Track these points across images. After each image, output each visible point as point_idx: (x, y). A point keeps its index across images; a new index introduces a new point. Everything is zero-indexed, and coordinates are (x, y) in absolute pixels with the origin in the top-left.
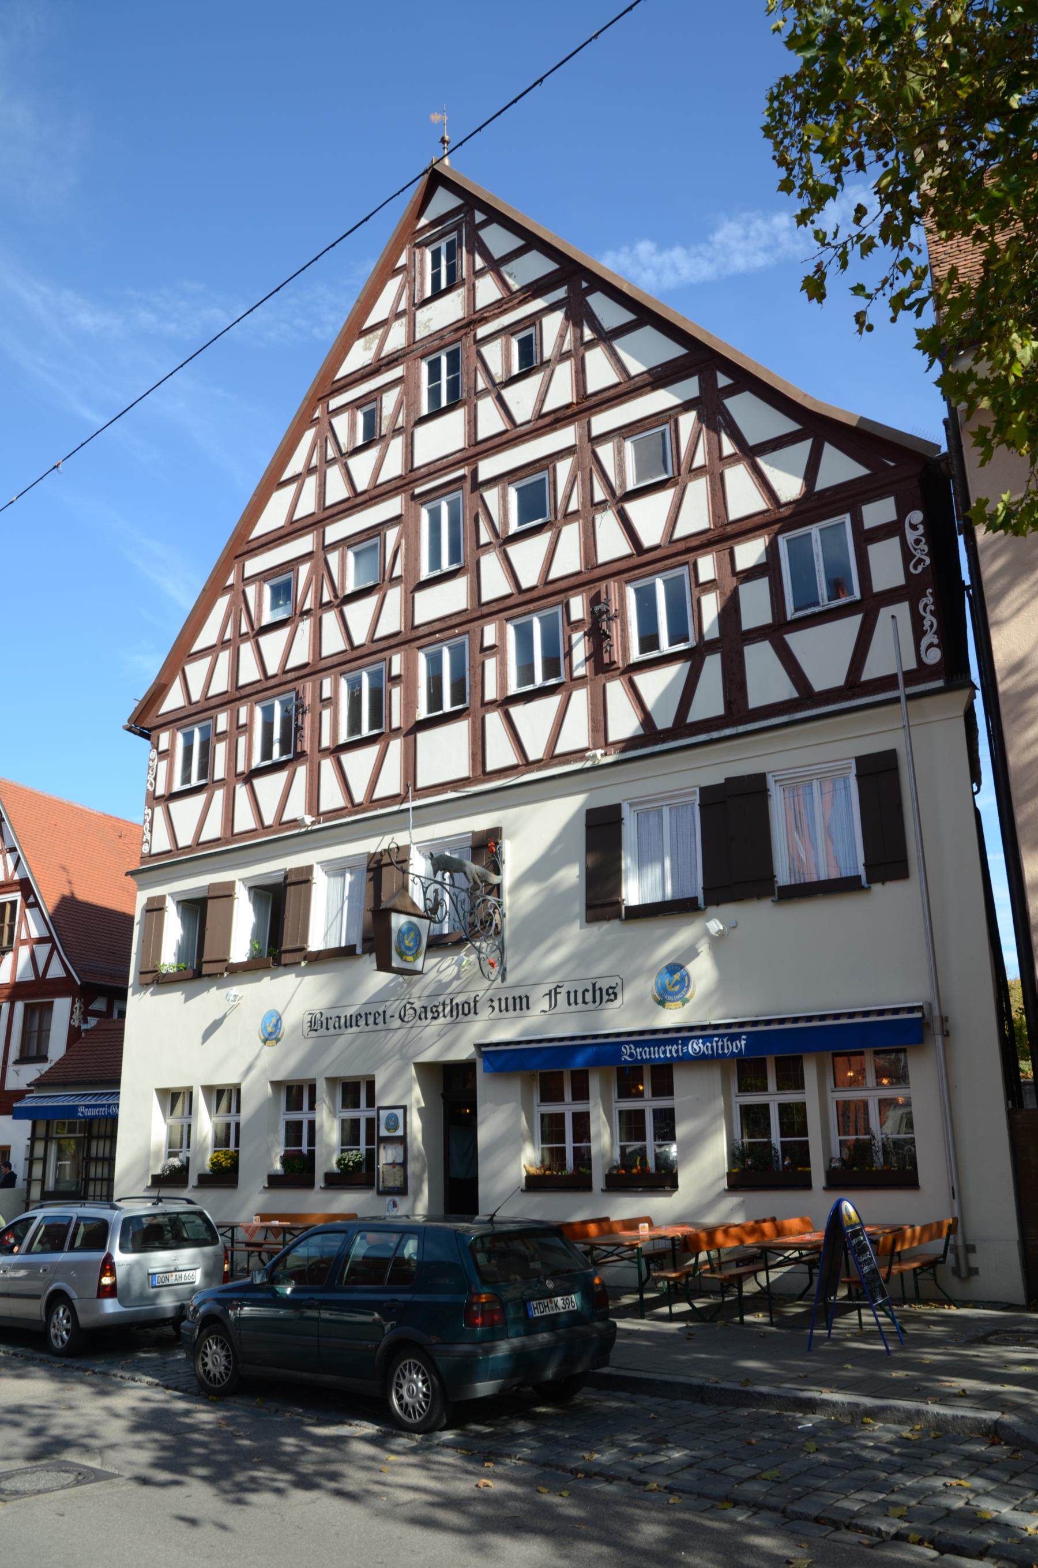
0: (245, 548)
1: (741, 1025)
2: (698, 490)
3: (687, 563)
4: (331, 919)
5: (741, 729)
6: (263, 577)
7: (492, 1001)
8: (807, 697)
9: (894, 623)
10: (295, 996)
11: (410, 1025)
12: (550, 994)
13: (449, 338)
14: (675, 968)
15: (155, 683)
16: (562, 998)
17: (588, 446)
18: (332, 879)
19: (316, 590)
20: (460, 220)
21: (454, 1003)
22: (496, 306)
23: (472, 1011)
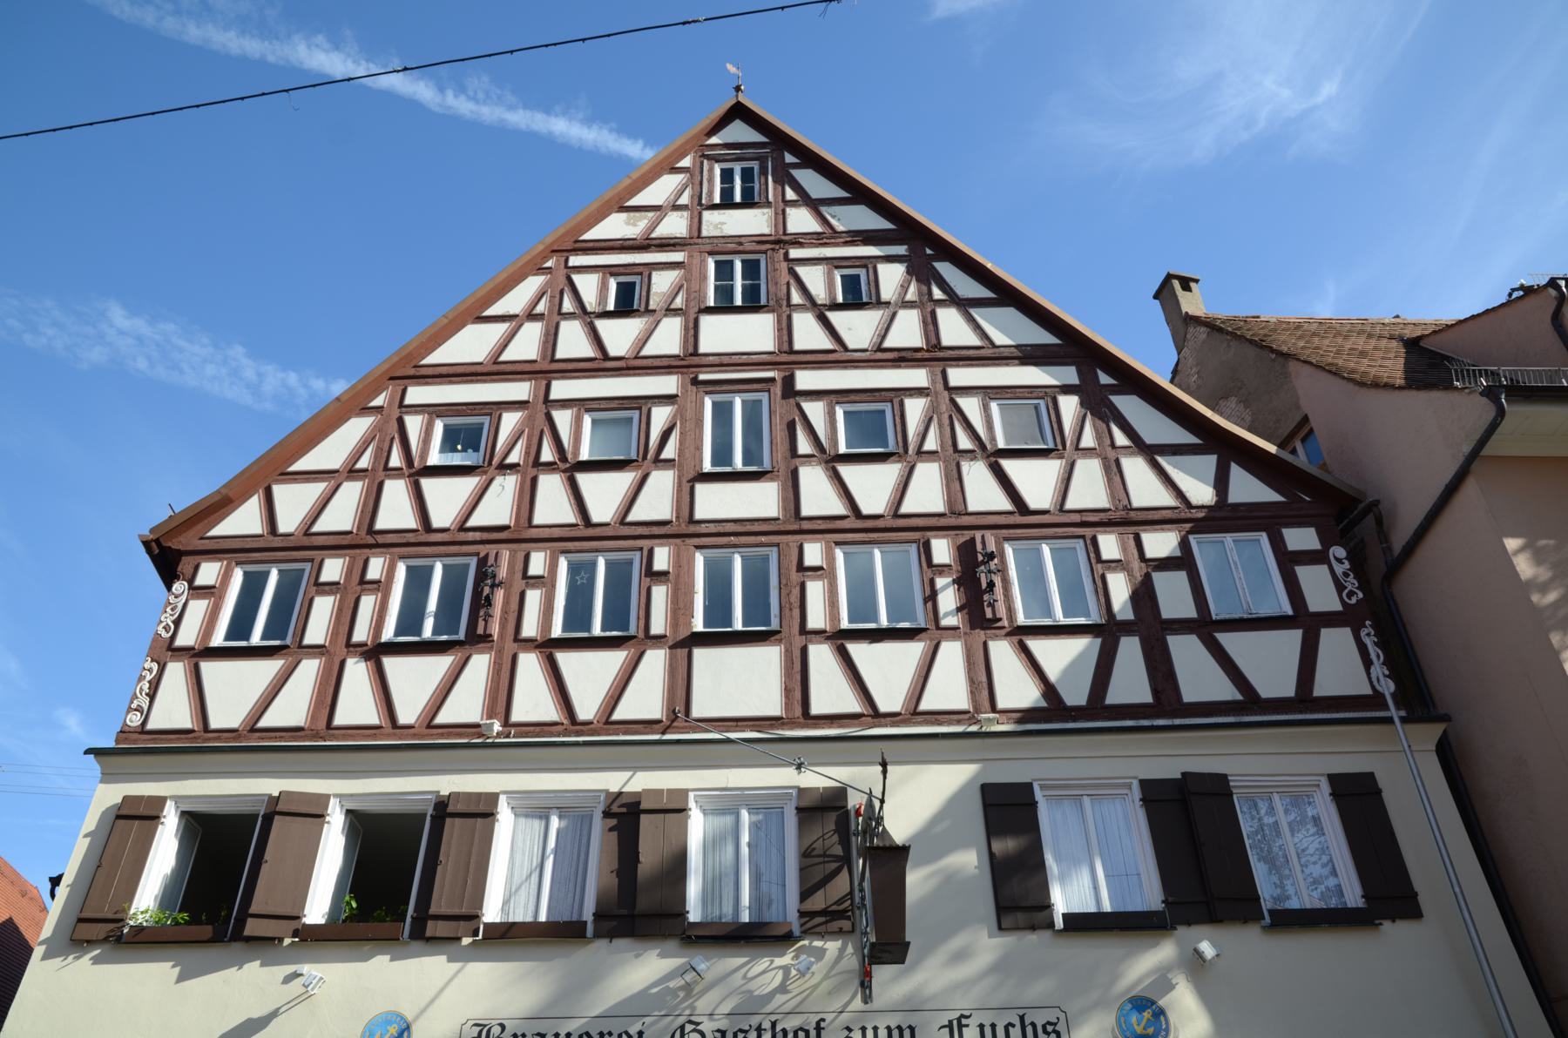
0: (412, 372)
2: (504, 490)
3: (312, 560)
4: (517, 881)
5: (1178, 722)
6: (433, 411)
7: (849, 1029)
9: (1337, 645)
12: (950, 1026)
13: (748, 246)
15: (218, 491)
17: (541, 408)
18: (522, 820)
19: (528, 447)
20: (772, 155)
21: (778, 1028)
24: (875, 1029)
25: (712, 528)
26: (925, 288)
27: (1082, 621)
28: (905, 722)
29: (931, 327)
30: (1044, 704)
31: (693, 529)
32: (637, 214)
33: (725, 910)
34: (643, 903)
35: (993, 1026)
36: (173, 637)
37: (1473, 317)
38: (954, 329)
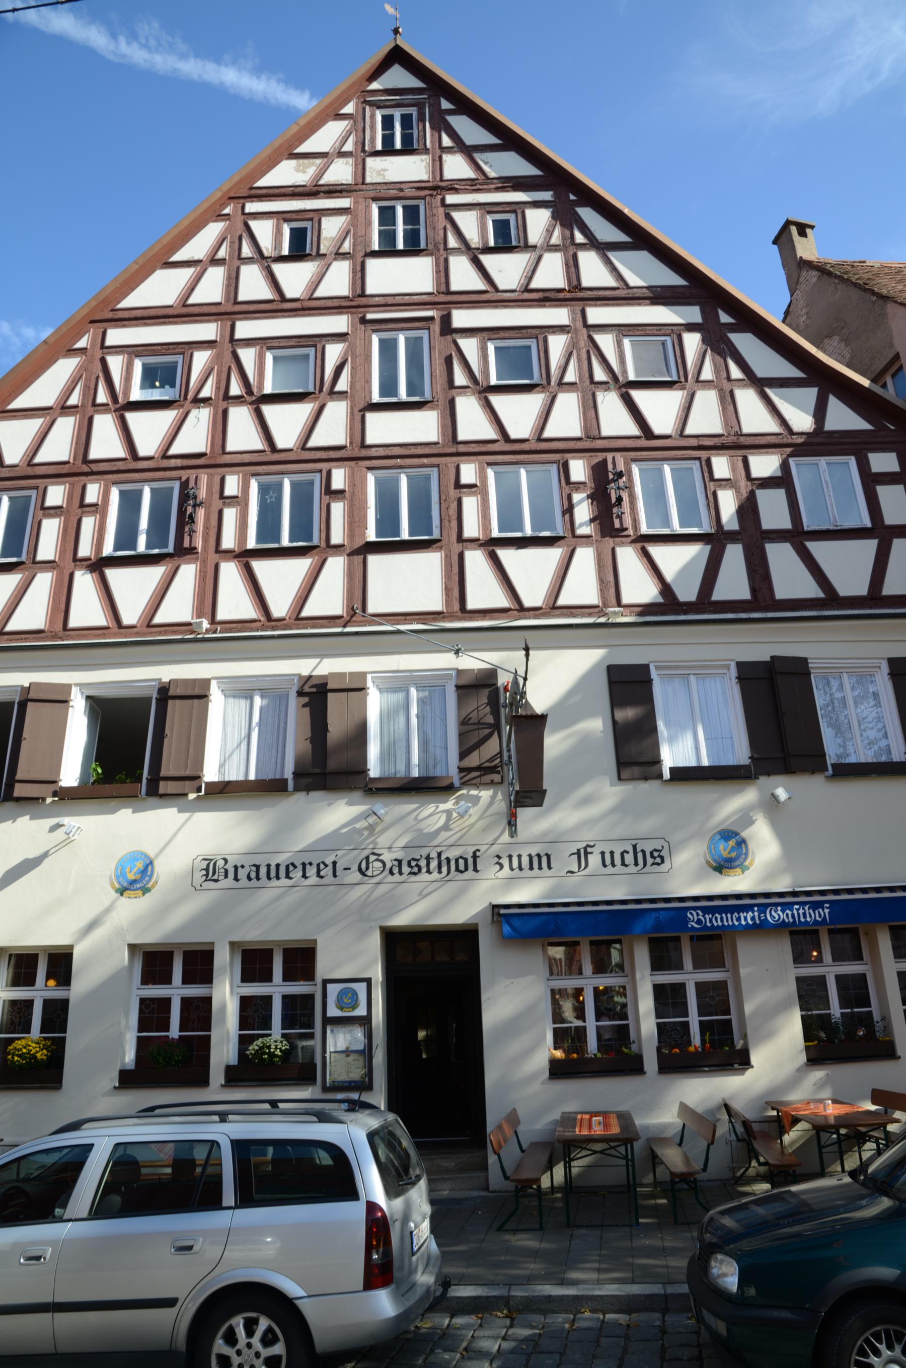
0: (110, 315)
1: (822, 893)
3: (37, 488)
5: (770, 615)
7: (499, 857)
10: (177, 838)
12: (578, 853)
16: (594, 860)
17: (228, 347)
18: (231, 700)
19: (218, 382)
21: (443, 857)
22: (469, 183)
23: (471, 867)
24: (520, 856)
25: (381, 452)
26: (568, 232)
28: (546, 615)
29: (573, 269)
30: (661, 600)
33: (398, 768)
34: (333, 764)
38: (593, 271)
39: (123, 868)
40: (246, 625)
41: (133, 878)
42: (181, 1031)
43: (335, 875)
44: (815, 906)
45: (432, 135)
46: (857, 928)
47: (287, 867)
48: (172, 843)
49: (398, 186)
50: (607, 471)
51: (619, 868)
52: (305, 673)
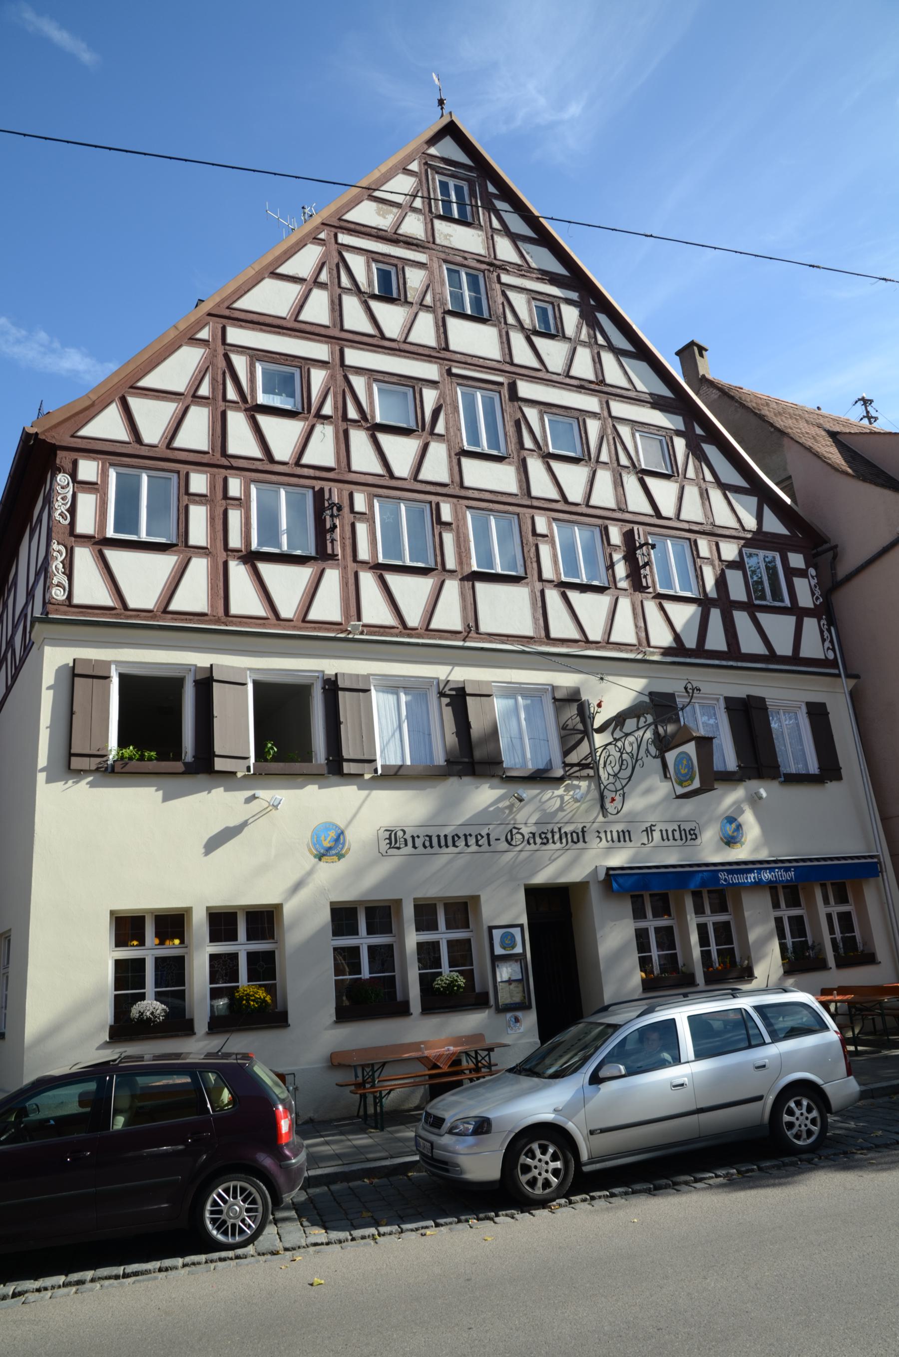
0: (227, 313)
1: (789, 861)
5: (740, 664)
7: (599, 832)
8: (772, 657)
10: (368, 813)
11: (518, 848)
12: (646, 830)
14: (731, 820)
16: (657, 835)
17: (221, 350)
19: (336, 403)
21: (563, 831)
23: (581, 839)
24: (611, 832)
25: (476, 495)
26: (592, 332)
27: (688, 594)
28: (154, 618)
29: (598, 365)
30: (674, 645)
31: (463, 493)
32: (385, 207)
33: (517, 760)
34: (478, 754)
35: (667, 831)
36: (72, 524)
37: (890, 433)
38: (613, 373)
39: (318, 837)
40: (387, 630)
41: (329, 845)
42: (370, 973)
43: (489, 845)
44: (787, 869)
45: (483, 214)
46: (844, 883)
47: (453, 837)
48: (358, 816)
49: (462, 254)
50: (635, 540)
51: (672, 842)
52: (443, 677)
